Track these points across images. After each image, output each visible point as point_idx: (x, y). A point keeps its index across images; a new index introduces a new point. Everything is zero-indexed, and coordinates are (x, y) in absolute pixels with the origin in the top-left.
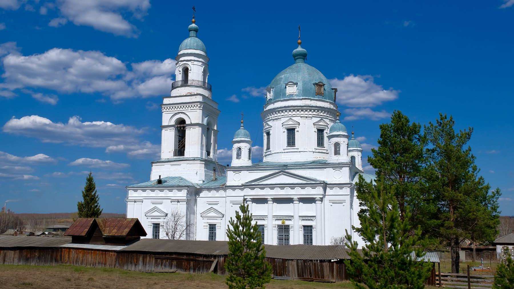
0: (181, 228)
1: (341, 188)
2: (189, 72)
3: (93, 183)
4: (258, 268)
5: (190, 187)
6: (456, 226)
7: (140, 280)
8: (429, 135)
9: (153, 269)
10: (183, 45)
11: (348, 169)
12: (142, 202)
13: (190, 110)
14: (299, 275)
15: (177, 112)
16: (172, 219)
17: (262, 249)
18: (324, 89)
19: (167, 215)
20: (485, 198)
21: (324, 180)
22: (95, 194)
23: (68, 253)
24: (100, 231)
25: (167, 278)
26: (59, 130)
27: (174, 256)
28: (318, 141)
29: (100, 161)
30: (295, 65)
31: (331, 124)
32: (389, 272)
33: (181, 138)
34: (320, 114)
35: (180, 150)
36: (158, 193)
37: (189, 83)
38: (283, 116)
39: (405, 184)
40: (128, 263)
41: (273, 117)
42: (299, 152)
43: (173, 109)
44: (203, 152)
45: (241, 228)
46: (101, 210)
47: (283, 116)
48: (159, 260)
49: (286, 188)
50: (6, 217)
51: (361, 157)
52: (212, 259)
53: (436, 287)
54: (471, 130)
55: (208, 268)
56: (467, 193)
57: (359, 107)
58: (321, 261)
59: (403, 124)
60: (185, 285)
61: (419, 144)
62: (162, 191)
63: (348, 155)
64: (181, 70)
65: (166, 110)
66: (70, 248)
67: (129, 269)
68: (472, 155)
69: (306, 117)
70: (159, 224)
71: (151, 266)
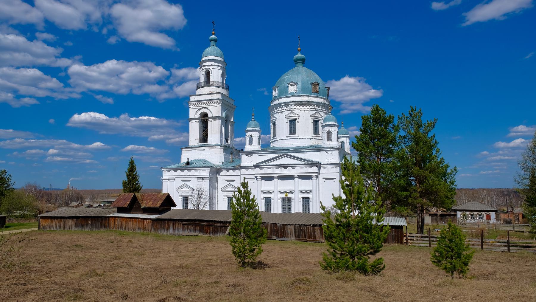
0: (204, 201)
1: (332, 167)
2: (210, 74)
3: (135, 165)
4: (255, 232)
5: (212, 168)
6: (421, 196)
7: (169, 241)
8: (402, 123)
9: (181, 233)
10: (205, 53)
11: (337, 152)
12: (174, 180)
13: (212, 105)
14: (296, 237)
15: (201, 107)
16: (197, 193)
17: (259, 217)
18: (319, 88)
19: (194, 190)
20: (445, 175)
21: (319, 161)
22: (136, 174)
23: (114, 221)
24: (139, 204)
25: (191, 240)
26: (113, 123)
27: (197, 223)
28: (314, 129)
29: (145, 147)
30: (296, 68)
31: (324, 116)
32: (356, 235)
33: (205, 128)
34: (315, 108)
35: (204, 138)
36: (186, 173)
37: (211, 83)
38: (286, 110)
39: (381, 164)
40: (161, 228)
41: (278, 111)
42: (299, 139)
43: (198, 105)
44: (222, 140)
45: (242, 201)
46: (141, 187)
47: (286, 110)
48: (185, 226)
49: (288, 168)
50: (70, 192)
51: (349, 143)
52: (228, 224)
53: (404, 245)
54: (436, 121)
55: (224, 232)
56: (433, 171)
57: (352, 103)
58: (313, 226)
59: (380, 115)
60: (205, 245)
61: (393, 131)
62: (189, 171)
63: (338, 141)
64: (204, 73)
65: (192, 106)
66: (115, 217)
67: (162, 233)
68: (436, 141)
69: (305, 111)
70: (188, 197)
71: (179, 230)
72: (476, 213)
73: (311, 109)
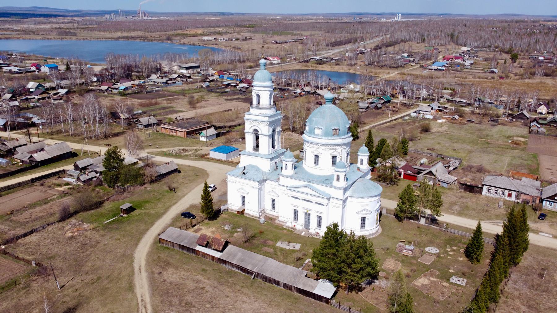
72: (500, 190)
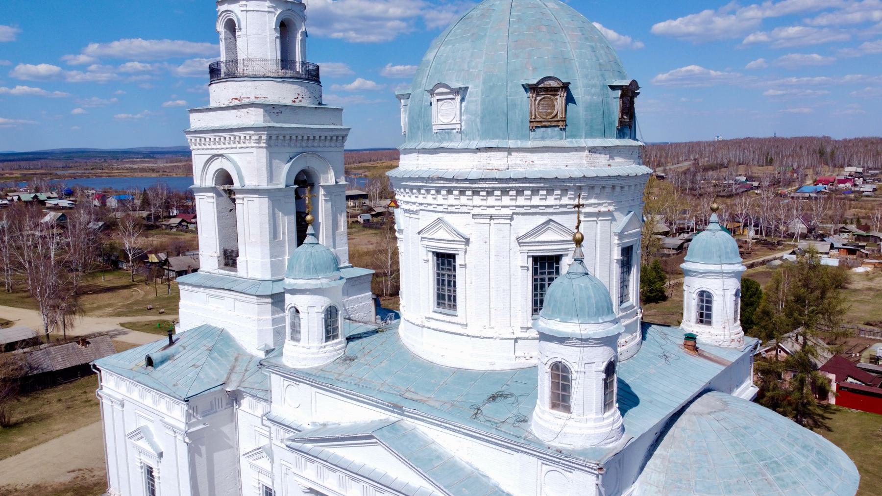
73: (522, 210)
